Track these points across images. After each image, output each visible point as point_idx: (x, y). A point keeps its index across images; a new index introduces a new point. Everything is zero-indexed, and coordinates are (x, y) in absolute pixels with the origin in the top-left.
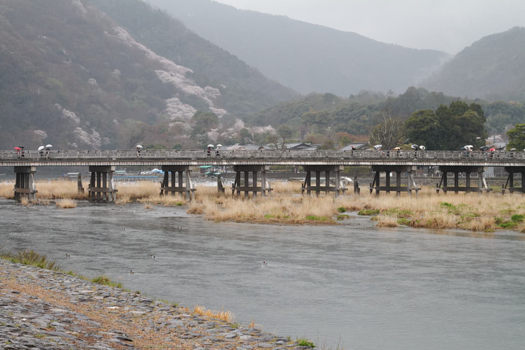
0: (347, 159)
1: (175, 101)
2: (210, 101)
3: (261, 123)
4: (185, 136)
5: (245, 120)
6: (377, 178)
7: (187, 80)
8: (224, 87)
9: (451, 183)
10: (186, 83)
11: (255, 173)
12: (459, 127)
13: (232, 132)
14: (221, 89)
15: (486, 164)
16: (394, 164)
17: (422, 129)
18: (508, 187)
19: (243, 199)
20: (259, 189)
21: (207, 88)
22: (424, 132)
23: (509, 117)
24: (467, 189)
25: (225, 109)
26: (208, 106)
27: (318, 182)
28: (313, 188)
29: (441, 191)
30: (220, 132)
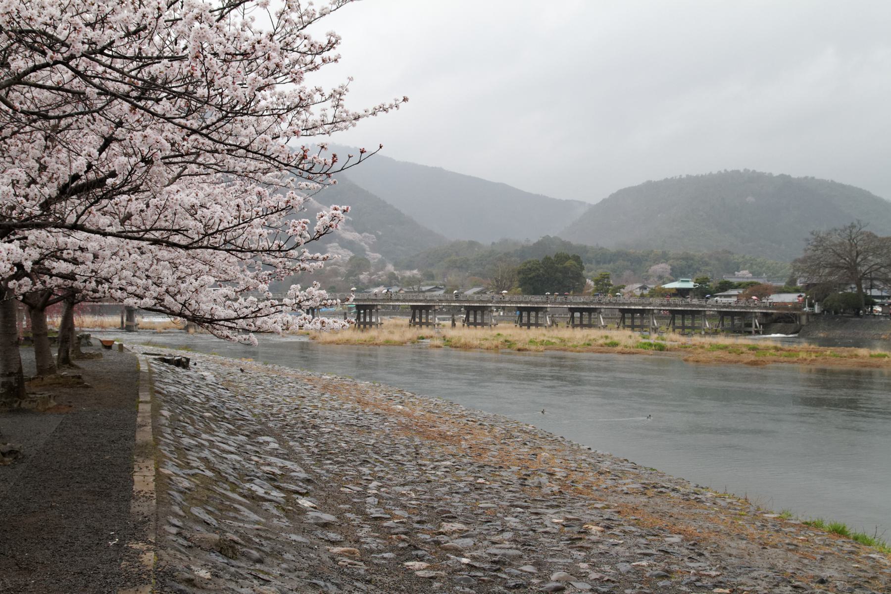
0: (441, 301)
1: (334, 247)
2: (367, 247)
3: (410, 267)
4: (339, 278)
5: (396, 265)
6: (572, 317)
7: (346, 227)
8: (380, 233)
9: (471, 319)
10: (345, 230)
11: (427, 311)
12: (560, 274)
13: (382, 275)
14: (378, 237)
15: (549, 306)
16: (478, 305)
17: (530, 276)
18: (671, 326)
19: (362, 331)
20: (373, 323)
21: (363, 234)
22: (531, 278)
23: (629, 264)
24: (483, 324)
25: (380, 254)
26: (364, 250)
27: (475, 319)
28: (417, 323)
29: (518, 326)
30: (371, 274)
